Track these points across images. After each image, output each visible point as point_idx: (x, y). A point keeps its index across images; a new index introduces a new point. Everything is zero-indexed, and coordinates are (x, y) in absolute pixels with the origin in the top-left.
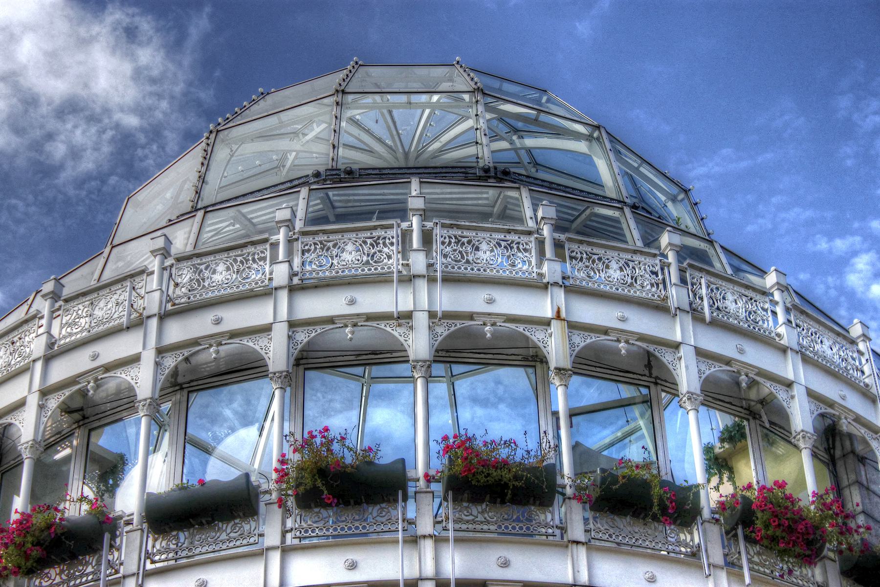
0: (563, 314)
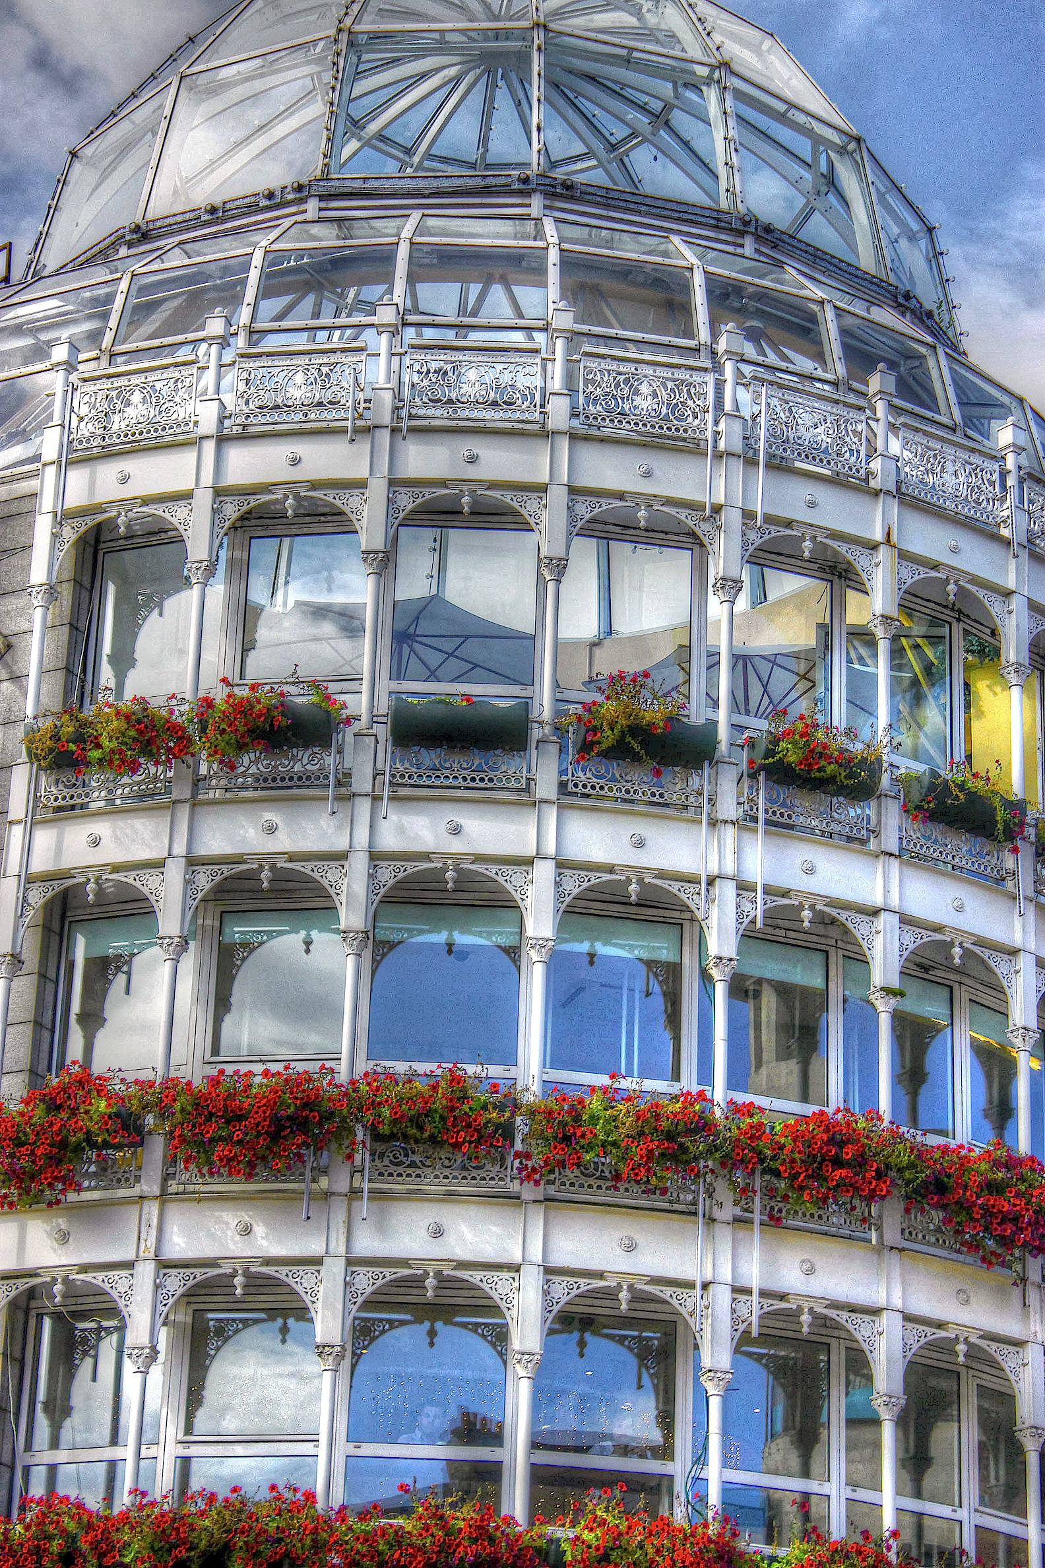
0: (894, 538)
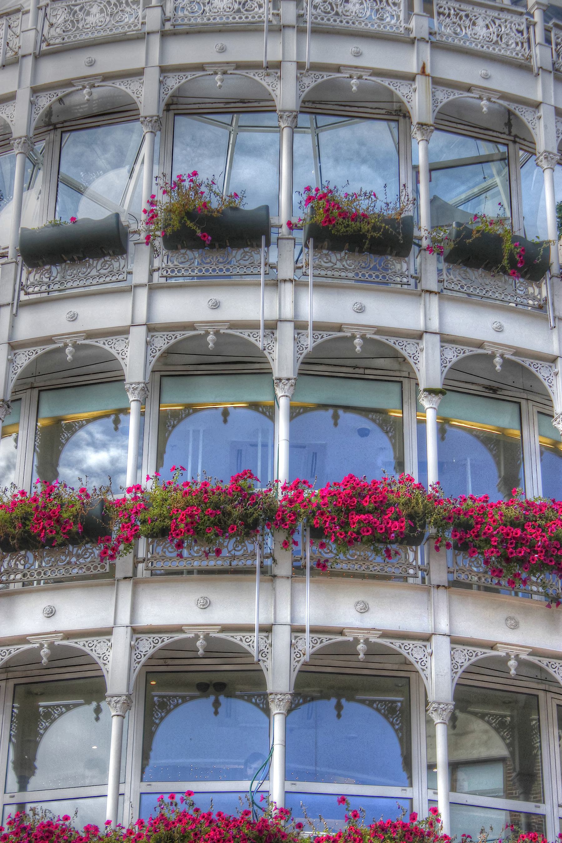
0: (428, 70)
